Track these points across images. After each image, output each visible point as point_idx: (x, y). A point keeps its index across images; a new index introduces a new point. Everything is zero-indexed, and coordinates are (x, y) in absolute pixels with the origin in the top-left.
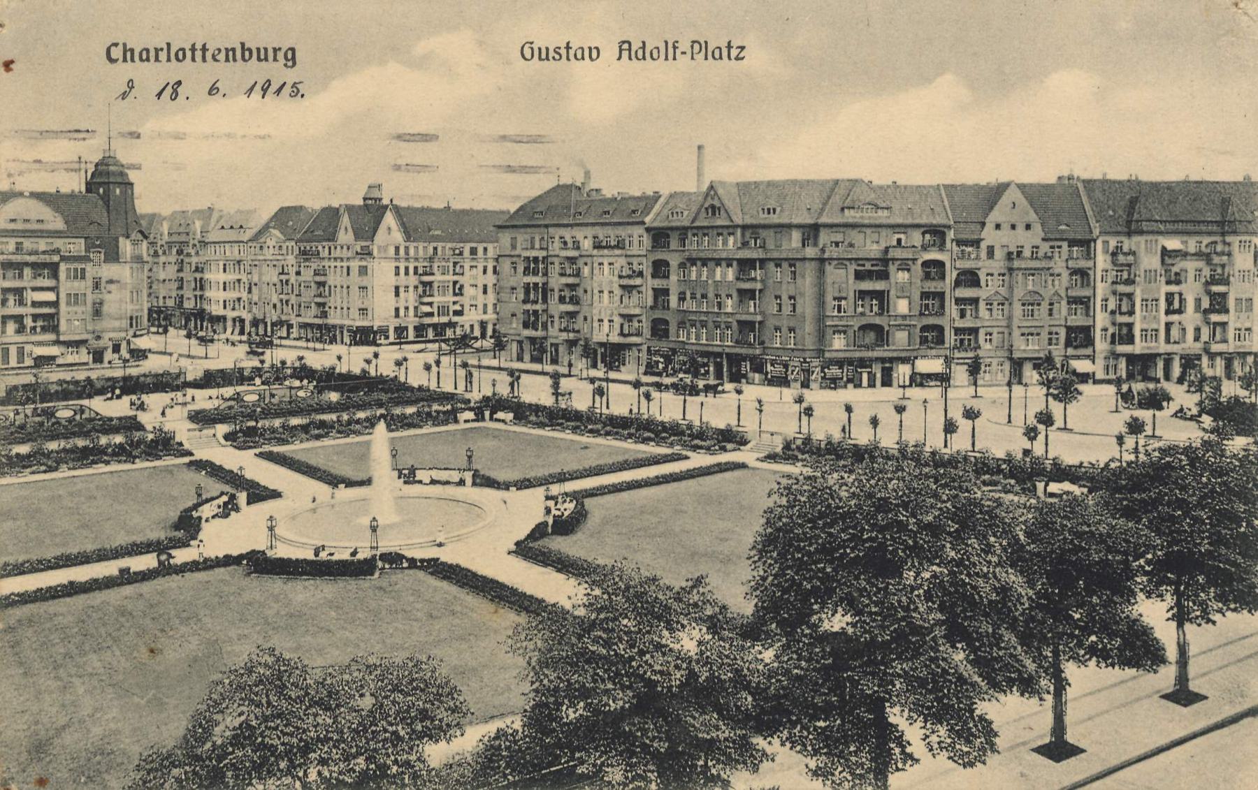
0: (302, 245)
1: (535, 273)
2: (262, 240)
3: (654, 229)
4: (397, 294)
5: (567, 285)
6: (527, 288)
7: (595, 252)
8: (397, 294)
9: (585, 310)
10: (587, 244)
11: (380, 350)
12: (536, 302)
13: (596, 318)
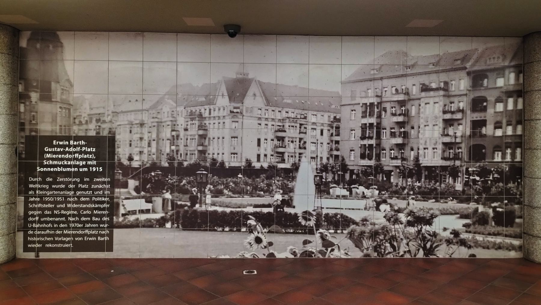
0: (189, 109)
1: (371, 115)
2: (160, 107)
3: (474, 72)
4: (259, 145)
5: (398, 123)
6: (364, 127)
7: (423, 94)
8: (259, 145)
9: (413, 143)
10: (415, 91)
11: (410, 145)
12: (371, 138)
13: (421, 147)
